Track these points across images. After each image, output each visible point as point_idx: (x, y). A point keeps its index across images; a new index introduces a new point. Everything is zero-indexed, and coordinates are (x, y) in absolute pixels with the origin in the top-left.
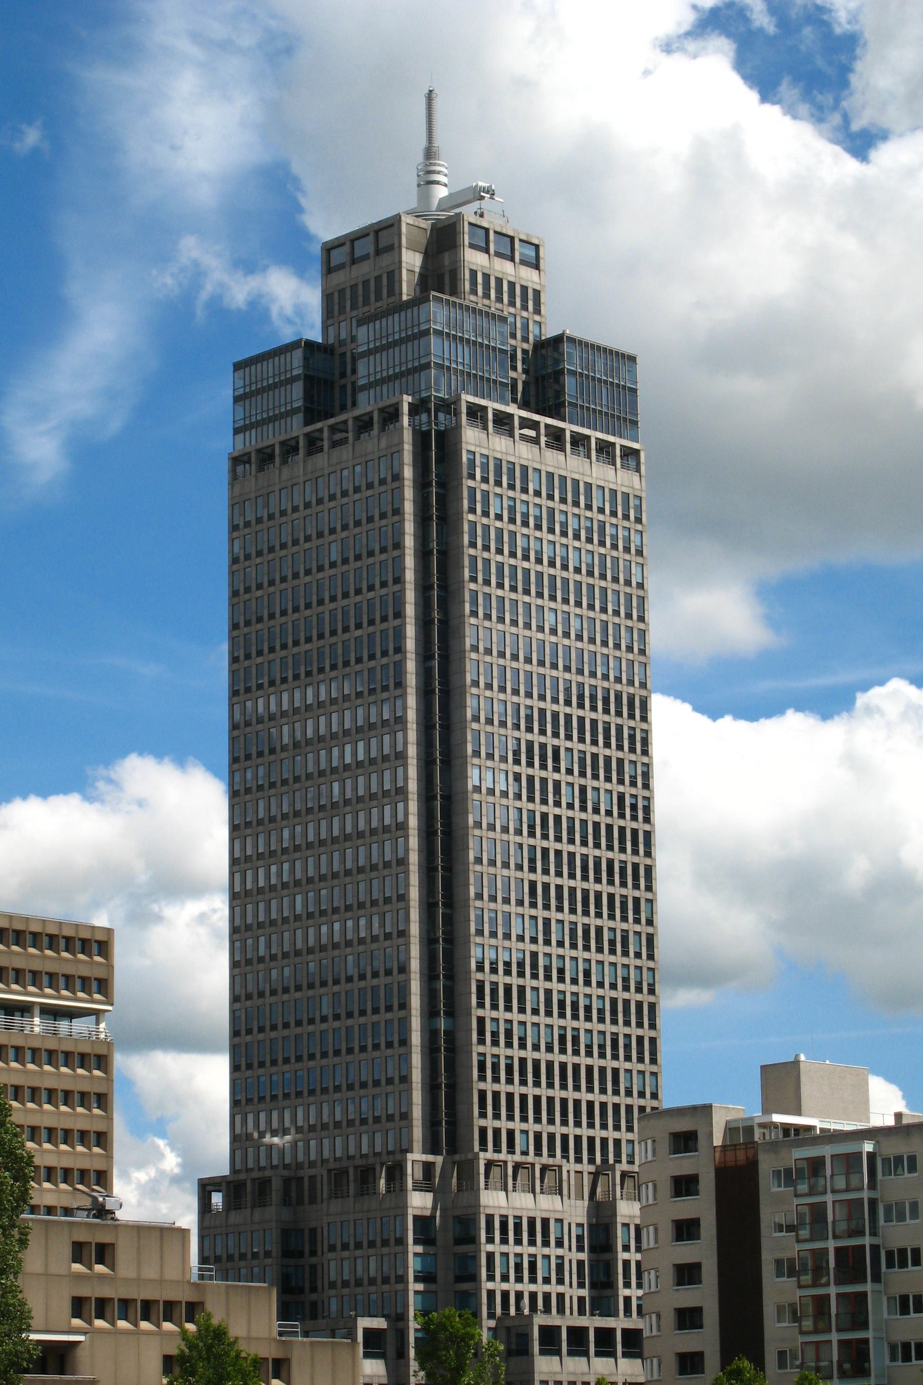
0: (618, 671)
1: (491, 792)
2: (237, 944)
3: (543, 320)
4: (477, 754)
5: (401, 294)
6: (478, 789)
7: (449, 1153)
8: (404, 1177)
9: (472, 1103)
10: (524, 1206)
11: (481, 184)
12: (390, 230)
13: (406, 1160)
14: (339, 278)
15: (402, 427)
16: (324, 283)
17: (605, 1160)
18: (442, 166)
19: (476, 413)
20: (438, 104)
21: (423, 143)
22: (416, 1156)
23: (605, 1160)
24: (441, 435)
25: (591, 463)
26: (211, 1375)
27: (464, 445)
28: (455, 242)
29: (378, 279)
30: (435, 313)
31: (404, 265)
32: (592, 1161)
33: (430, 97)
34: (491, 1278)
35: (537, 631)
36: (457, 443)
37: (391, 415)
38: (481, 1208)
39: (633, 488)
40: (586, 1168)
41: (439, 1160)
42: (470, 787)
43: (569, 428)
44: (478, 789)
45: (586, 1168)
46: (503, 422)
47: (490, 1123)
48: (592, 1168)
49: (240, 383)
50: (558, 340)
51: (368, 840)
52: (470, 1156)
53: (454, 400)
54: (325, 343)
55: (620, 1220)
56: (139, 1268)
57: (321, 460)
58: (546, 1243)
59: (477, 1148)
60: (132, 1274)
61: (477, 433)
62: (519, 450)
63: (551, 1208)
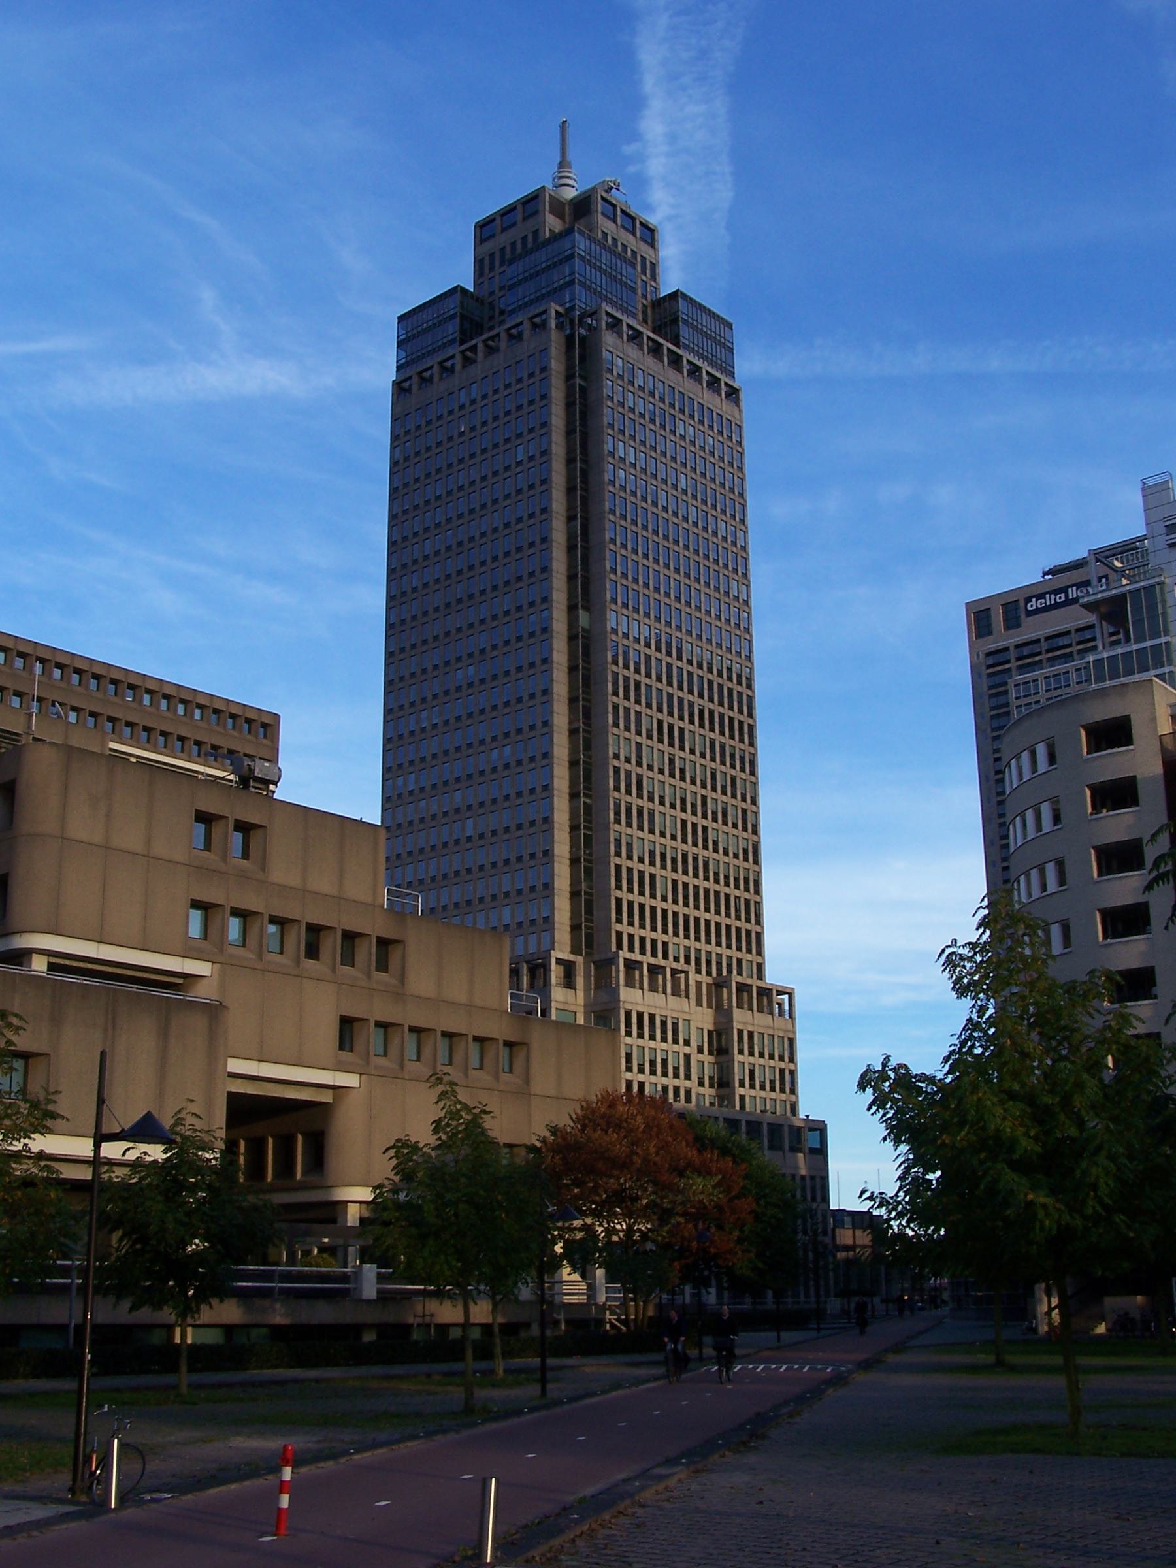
0: (617, 748)
1: (626, 636)
4: (614, 601)
6: (614, 631)
11: (608, 179)
14: (489, 246)
15: (551, 329)
16: (478, 234)
19: (615, 324)
20: (570, 131)
21: (558, 160)
22: (562, 951)
24: (583, 339)
26: (754, 1206)
29: (524, 238)
32: (709, 973)
33: (384, 1153)
34: (629, 1069)
35: (622, 607)
37: (539, 326)
40: (704, 979)
42: (609, 629)
44: (614, 631)
45: (704, 979)
48: (709, 980)
49: (403, 354)
55: (736, 1026)
57: (476, 371)
58: (675, 1041)
63: (680, 1009)
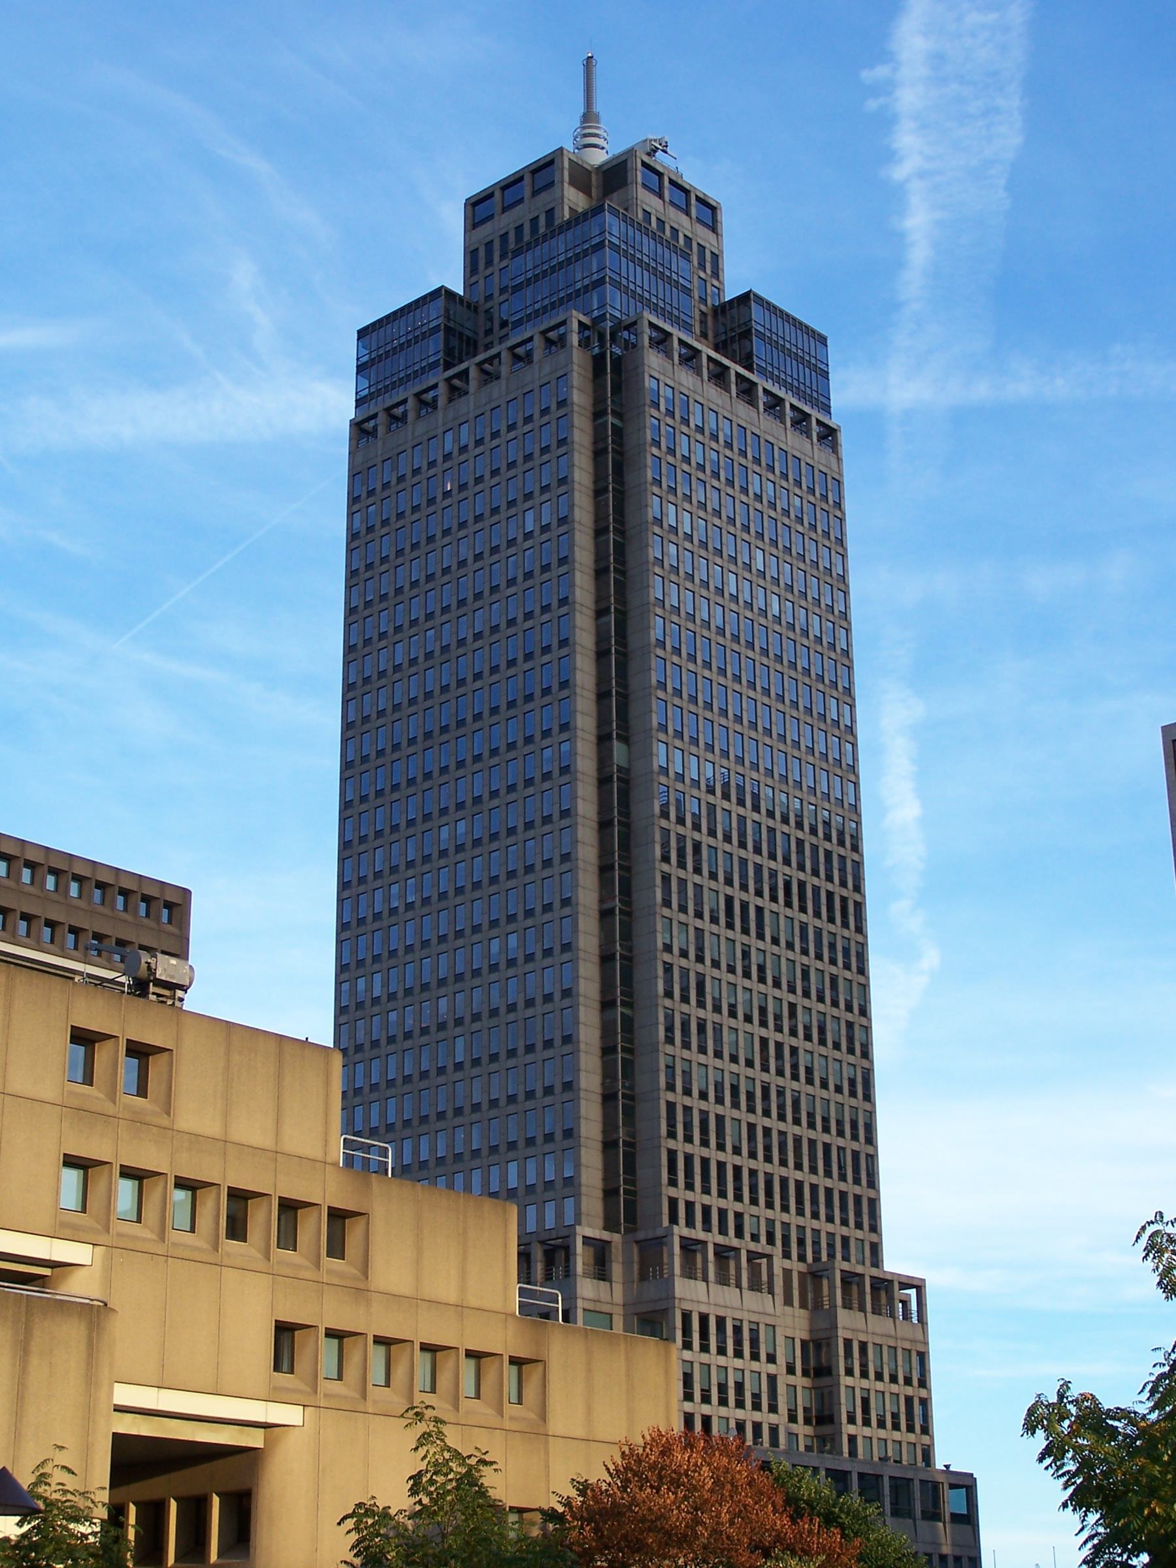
2: (345, 986)
3: (721, 287)
5: (563, 216)
6: (665, 771)
7: (628, 1231)
8: (571, 1258)
9: (660, 1166)
10: (728, 1304)
12: (291, 1241)
13: (575, 1234)
14: (485, 231)
17: (817, 1258)
18: (603, 128)
19: (662, 340)
23: (817, 1258)
25: (786, 429)
27: (646, 368)
28: (626, 179)
30: (610, 225)
31: (566, 200)
32: (802, 1258)
36: (637, 367)
38: (677, 1301)
39: (831, 469)
41: (616, 1238)
43: (762, 383)
45: (796, 1266)
46: (690, 357)
47: (681, 1194)
48: (802, 1267)
50: (745, 299)
51: (521, 837)
52: (660, 1232)
53: (632, 320)
54: (468, 296)
55: (842, 1334)
56: (226, 1115)
59: (666, 1222)
60: (210, 1126)
61: (661, 361)
62: (708, 391)
63: (761, 1310)
